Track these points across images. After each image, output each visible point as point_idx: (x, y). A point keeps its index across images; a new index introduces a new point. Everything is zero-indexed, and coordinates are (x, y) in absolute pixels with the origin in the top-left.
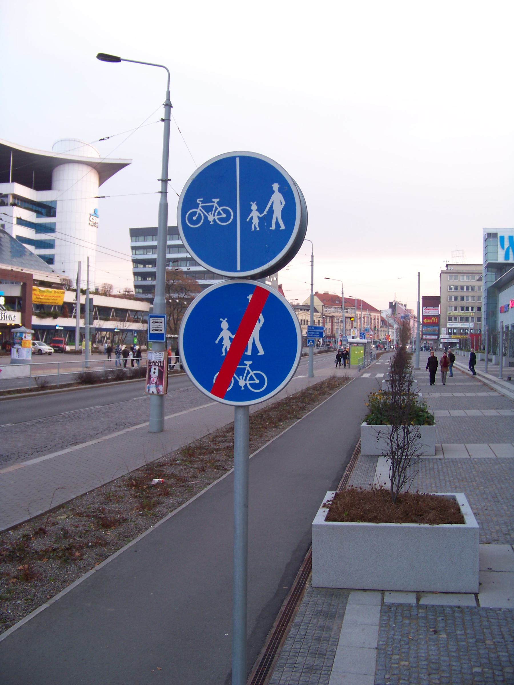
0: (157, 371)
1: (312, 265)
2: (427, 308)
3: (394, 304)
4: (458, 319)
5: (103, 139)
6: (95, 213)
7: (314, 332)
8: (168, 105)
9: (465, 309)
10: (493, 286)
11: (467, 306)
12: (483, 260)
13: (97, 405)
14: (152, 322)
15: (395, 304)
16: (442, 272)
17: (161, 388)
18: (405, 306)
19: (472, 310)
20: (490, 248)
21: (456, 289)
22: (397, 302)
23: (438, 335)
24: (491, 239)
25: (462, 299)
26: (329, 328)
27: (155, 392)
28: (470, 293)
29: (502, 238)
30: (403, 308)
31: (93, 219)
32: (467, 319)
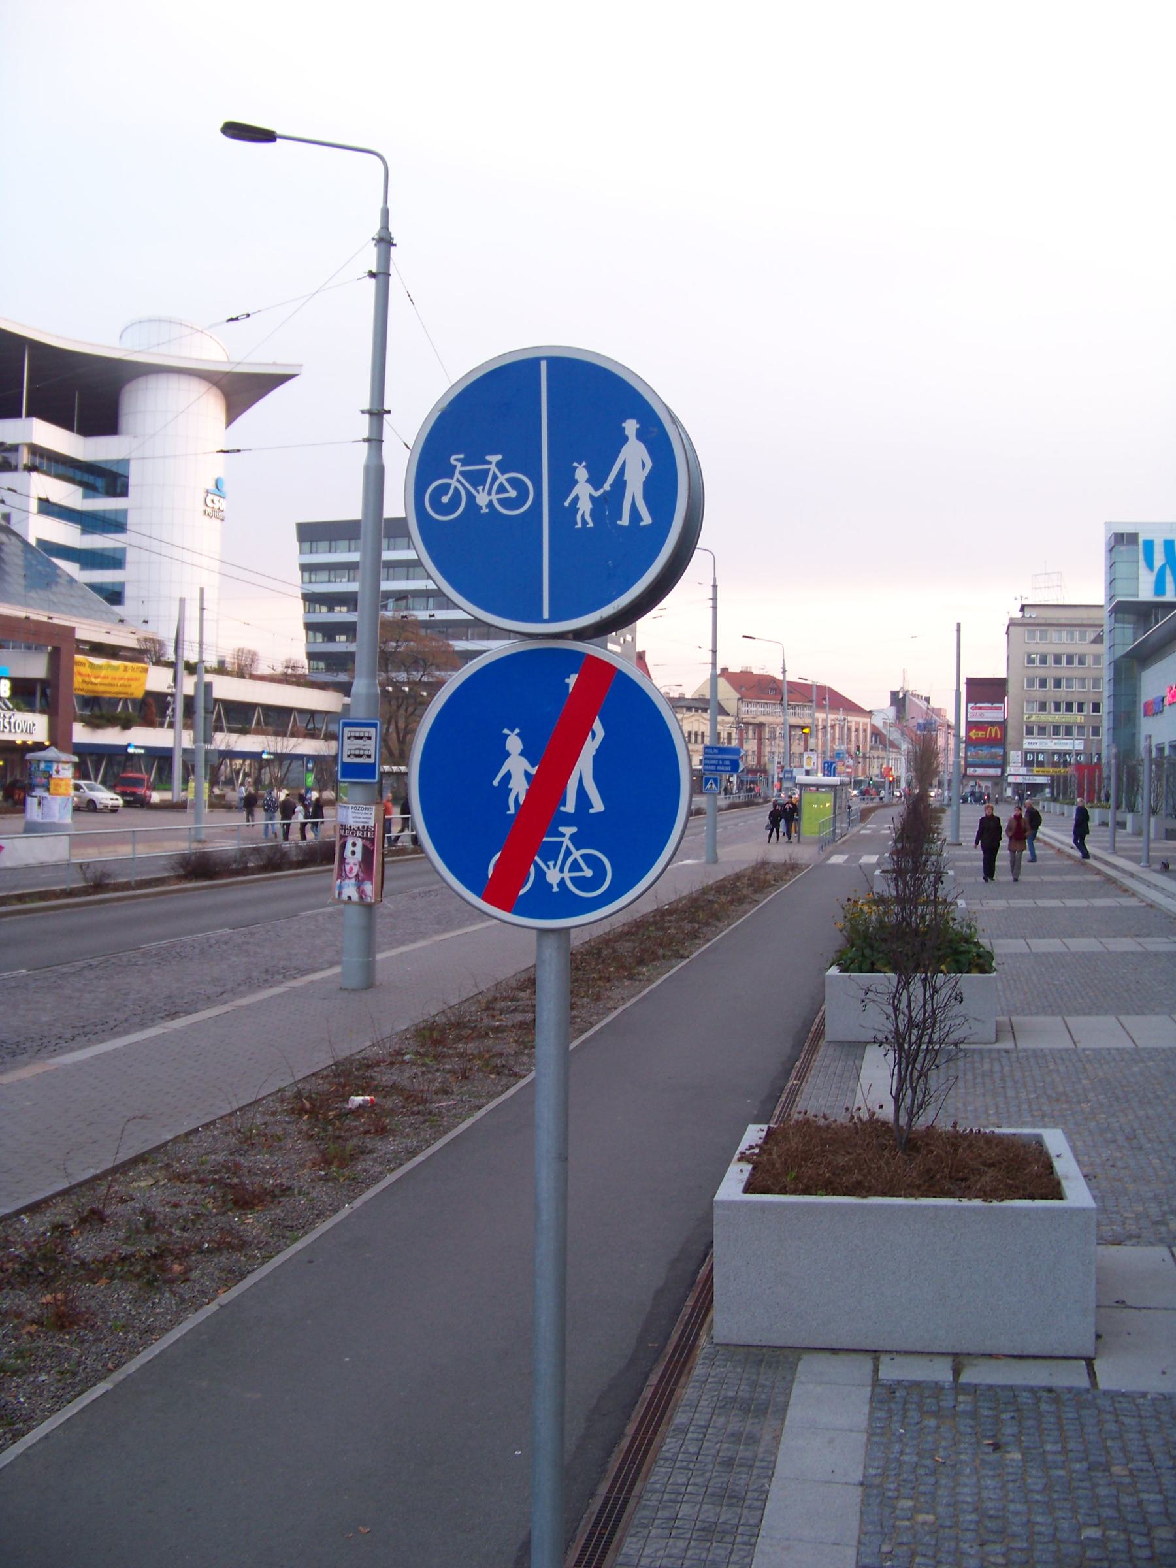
0: (359, 849)
1: (715, 608)
2: (978, 705)
3: (901, 695)
4: (1049, 730)
5: (237, 319)
6: (217, 488)
7: (719, 760)
8: (385, 241)
9: (1063, 707)
10: (1128, 655)
11: (1069, 699)
12: (1106, 595)
13: (221, 926)
14: (349, 738)
15: (905, 696)
16: (1012, 623)
17: (369, 888)
18: (927, 700)
19: (1080, 710)
20: (1121, 569)
21: (1044, 660)
22: (908, 691)
23: (1003, 766)
24: (1123, 548)
25: (1058, 683)
26: (753, 752)
27: (355, 897)
28: (1076, 670)
29: (1149, 545)
30: (923, 704)
31: (213, 501)
32: (1069, 731)
